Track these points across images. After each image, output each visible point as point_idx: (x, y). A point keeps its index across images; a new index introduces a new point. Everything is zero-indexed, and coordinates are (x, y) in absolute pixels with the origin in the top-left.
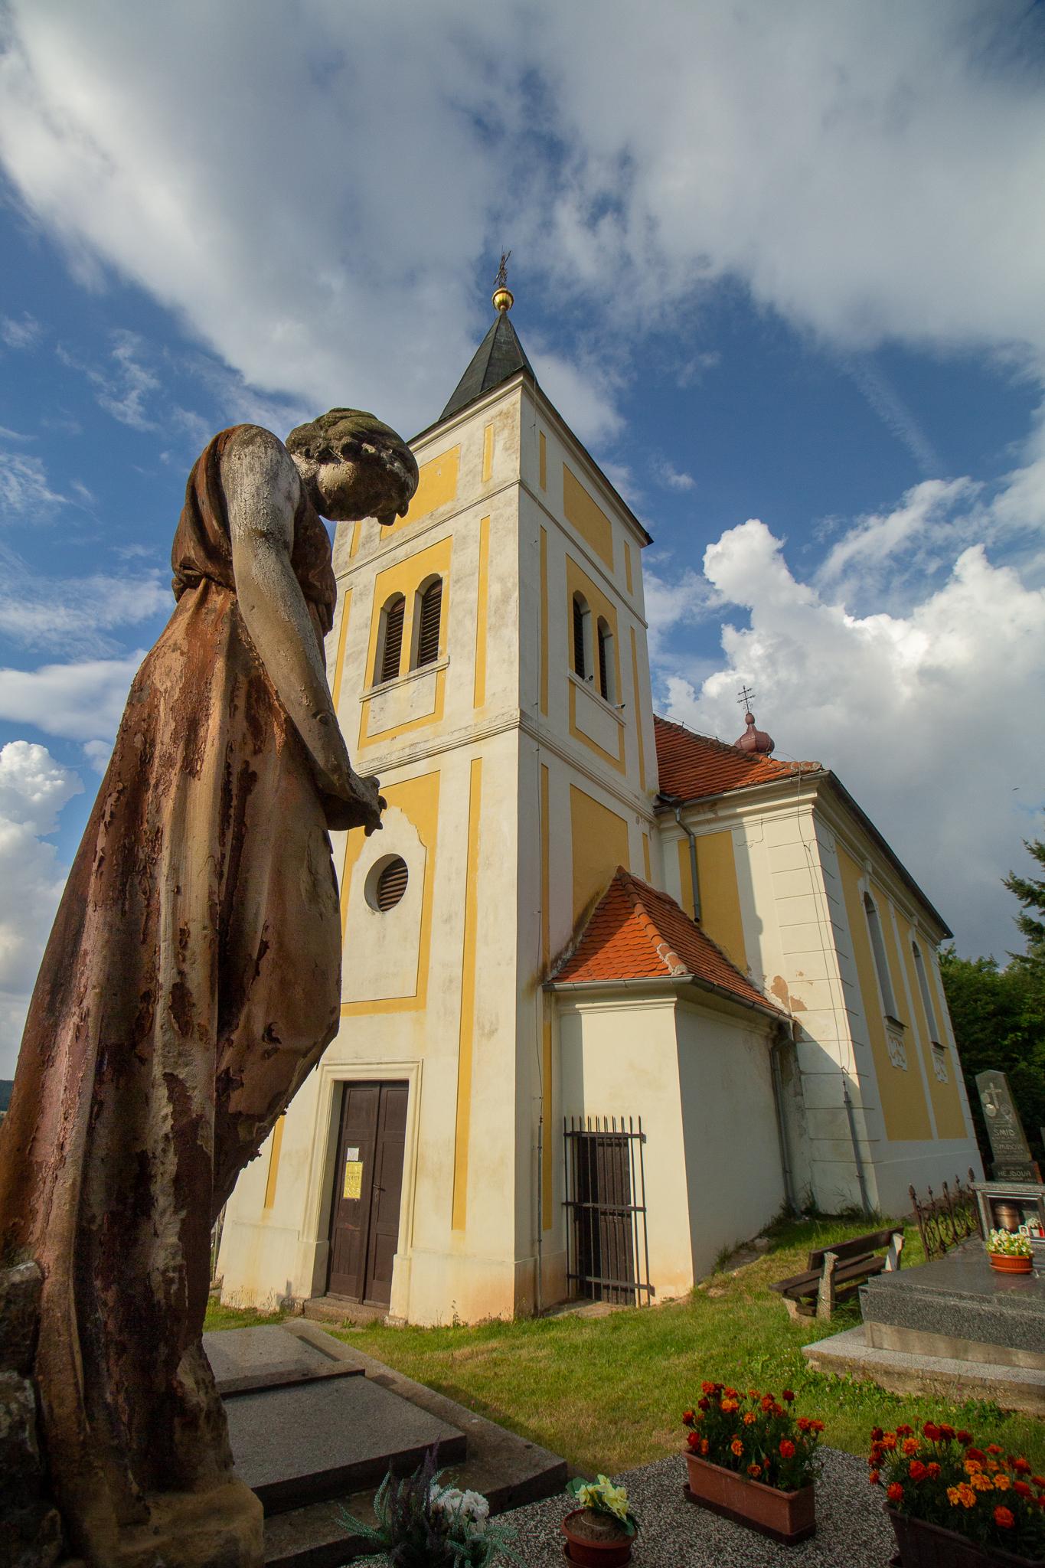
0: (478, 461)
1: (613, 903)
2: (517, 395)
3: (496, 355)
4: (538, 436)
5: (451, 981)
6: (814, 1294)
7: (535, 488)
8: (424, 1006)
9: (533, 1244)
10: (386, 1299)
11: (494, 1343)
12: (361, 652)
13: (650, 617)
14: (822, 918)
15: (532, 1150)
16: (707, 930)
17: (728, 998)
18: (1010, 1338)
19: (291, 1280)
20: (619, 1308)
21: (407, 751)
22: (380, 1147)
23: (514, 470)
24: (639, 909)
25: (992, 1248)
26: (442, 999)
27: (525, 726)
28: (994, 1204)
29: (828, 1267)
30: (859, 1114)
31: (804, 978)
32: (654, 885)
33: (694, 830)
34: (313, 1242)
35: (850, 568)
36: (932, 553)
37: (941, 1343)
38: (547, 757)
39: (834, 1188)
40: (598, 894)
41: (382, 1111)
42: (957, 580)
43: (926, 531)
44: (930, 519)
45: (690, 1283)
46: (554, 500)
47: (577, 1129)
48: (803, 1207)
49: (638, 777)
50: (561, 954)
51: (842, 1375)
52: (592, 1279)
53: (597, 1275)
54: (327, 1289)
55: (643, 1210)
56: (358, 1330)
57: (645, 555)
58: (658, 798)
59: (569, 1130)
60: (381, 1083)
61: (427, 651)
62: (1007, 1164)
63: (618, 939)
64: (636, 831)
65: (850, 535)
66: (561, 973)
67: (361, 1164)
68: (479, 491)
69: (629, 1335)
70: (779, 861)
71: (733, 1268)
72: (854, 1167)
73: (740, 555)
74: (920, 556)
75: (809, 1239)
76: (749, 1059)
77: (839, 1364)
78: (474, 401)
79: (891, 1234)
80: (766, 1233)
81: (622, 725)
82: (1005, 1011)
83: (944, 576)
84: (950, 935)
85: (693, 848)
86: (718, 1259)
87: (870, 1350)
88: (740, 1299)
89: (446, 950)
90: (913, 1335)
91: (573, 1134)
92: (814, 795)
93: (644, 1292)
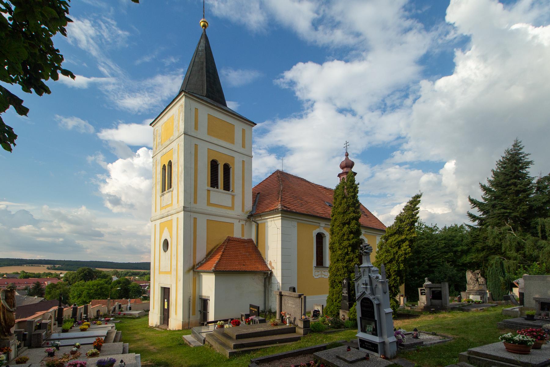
2: (184, 97)
16: (259, 249)
26: (174, 273)
34: (159, 316)
61: (170, 186)
66: (194, 270)
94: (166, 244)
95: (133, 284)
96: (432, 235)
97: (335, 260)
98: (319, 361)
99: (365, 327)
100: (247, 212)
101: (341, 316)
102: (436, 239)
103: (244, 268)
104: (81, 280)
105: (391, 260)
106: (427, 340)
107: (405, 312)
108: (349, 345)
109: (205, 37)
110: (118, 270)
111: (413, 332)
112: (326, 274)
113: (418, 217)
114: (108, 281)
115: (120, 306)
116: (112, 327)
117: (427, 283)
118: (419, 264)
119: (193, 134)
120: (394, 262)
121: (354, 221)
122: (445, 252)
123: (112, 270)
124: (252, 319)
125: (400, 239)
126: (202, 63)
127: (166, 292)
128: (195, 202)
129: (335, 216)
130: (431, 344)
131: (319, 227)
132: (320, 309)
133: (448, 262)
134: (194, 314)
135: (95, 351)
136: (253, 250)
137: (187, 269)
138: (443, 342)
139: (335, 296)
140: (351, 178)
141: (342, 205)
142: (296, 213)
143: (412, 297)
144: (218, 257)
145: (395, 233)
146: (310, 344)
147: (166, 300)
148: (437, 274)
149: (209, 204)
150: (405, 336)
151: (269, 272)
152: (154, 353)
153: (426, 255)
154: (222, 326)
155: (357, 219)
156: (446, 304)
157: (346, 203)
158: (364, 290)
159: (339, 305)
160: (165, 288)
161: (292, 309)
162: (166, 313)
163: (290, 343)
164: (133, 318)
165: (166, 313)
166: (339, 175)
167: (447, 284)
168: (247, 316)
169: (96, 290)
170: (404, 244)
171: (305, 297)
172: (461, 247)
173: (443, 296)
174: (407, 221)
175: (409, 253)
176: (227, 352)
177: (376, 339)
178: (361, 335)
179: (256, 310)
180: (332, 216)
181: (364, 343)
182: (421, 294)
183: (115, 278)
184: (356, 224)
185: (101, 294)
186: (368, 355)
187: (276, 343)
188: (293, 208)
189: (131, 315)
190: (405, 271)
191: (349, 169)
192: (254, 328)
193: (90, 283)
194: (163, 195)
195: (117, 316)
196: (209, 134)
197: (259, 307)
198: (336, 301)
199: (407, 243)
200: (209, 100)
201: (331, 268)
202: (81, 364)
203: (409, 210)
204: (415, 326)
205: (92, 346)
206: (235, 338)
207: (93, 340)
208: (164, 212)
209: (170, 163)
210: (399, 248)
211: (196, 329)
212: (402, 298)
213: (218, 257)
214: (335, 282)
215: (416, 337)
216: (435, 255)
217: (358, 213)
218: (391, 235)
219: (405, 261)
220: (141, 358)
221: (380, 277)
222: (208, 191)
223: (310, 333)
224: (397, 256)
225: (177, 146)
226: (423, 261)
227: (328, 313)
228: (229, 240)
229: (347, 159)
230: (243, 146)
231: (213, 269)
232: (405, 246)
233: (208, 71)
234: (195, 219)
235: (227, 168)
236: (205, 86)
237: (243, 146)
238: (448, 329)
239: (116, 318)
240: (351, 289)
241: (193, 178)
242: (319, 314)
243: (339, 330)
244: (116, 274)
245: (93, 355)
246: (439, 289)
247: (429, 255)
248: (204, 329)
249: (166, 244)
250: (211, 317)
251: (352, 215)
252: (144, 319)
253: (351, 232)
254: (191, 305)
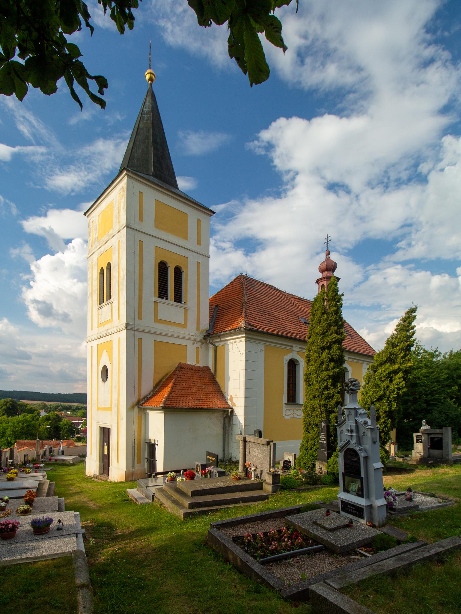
2: (126, 178)
3: (141, 126)
16: (218, 380)
21: (106, 332)
26: (115, 409)
34: (98, 463)
38: (139, 335)
40: (167, 374)
66: (139, 405)
92: (244, 335)
94: (105, 372)
95: (65, 420)
96: (432, 362)
97: (312, 396)
98: (292, 527)
99: (349, 485)
100: (202, 331)
101: (317, 469)
102: (438, 367)
103: (199, 404)
104: (3, 415)
105: (380, 396)
106: (423, 503)
107: (397, 465)
108: (329, 507)
109: (151, 94)
110: (47, 403)
111: (406, 492)
112: (299, 414)
113: (415, 340)
114: (35, 416)
115: (51, 449)
116: (44, 476)
117: (425, 427)
118: (415, 401)
119: (137, 227)
120: (384, 401)
121: (337, 345)
122: (447, 386)
123: (40, 402)
124: (209, 471)
125: (391, 369)
126: (148, 131)
127: (105, 434)
128: (140, 318)
129: (312, 338)
130: (428, 508)
131: (292, 351)
132: (291, 458)
133: (452, 398)
134: (139, 462)
135: (26, 507)
136: (210, 380)
137: (131, 404)
138: (442, 506)
139: (309, 443)
140: (333, 287)
141: (321, 324)
142: (264, 333)
143: (405, 445)
144: (167, 390)
145: (385, 362)
146: (279, 504)
147: (105, 444)
148: (436, 414)
149: (157, 320)
150: (397, 498)
151: (230, 410)
152: (93, 511)
153: (424, 390)
154: (173, 479)
155: (339, 342)
156: (448, 455)
157: (326, 320)
158: (349, 438)
159: (315, 455)
160: (104, 428)
161: (258, 459)
162: (106, 461)
163: (256, 503)
164: (67, 465)
165: (106, 461)
166: (318, 282)
167: (450, 429)
168: (204, 467)
169: (22, 428)
170: (397, 377)
171: (274, 445)
173: (444, 445)
174: (401, 345)
175: (403, 388)
176: (181, 513)
177: (362, 502)
178: (344, 496)
179: (214, 459)
180: (309, 338)
181: (347, 506)
182: (417, 442)
183: (43, 414)
184: (339, 349)
185: (28, 433)
186: (351, 522)
187: (239, 503)
188: (261, 327)
189: (64, 460)
190: (398, 411)
191: (331, 273)
192: (213, 483)
193: (16, 418)
194: (101, 308)
195: (50, 462)
196: (156, 226)
197: (218, 456)
198: (311, 449)
199: (401, 374)
200: (156, 180)
201: (306, 407)
202: (13, 524)
203: (401, 330)
204: (409, 484)
205: (22, 501)
206: (190, 494)
207: (24, 493)
208: (103, 330)
209: (109, 266)
210: (391, 381)
211: (142, 482)
212: (392, 446)
213: (167, 390)
214: (310, 425)
215: (410, 499)
216: (435, 389)
217: (341, 334)
218: (381, 364)
219: (398, 398)
220: (81, 517)
221: (369, 422)
222: (156, 302)
223: (280, 490)
224: (388, 393)
225: (117, 243)
226: (420, 398)
227: (302, 464)
228: (181, 368)
229: (328, 259)
230: (199, 243)
231: (162, 405)
232: (398, 378)
233: (155, 141)
234: (140, 339)
235: (178, 272)
236: (151, 161)
237: (199, 243)
238: (449, 489)
239: (48, 465)
240: (332, 435)
241: (137, 286)
242: (290, 465)
243: (315, 486)
244: (44, 408)
245: (25, 512)
246: (440, 436)
247: (427, 389)
248: (151, 482)
249: (105, 372)
250: (160, 467)
251: (334, 336)
252: (80, 466)
253: (332, 360)
254: (136, 451)
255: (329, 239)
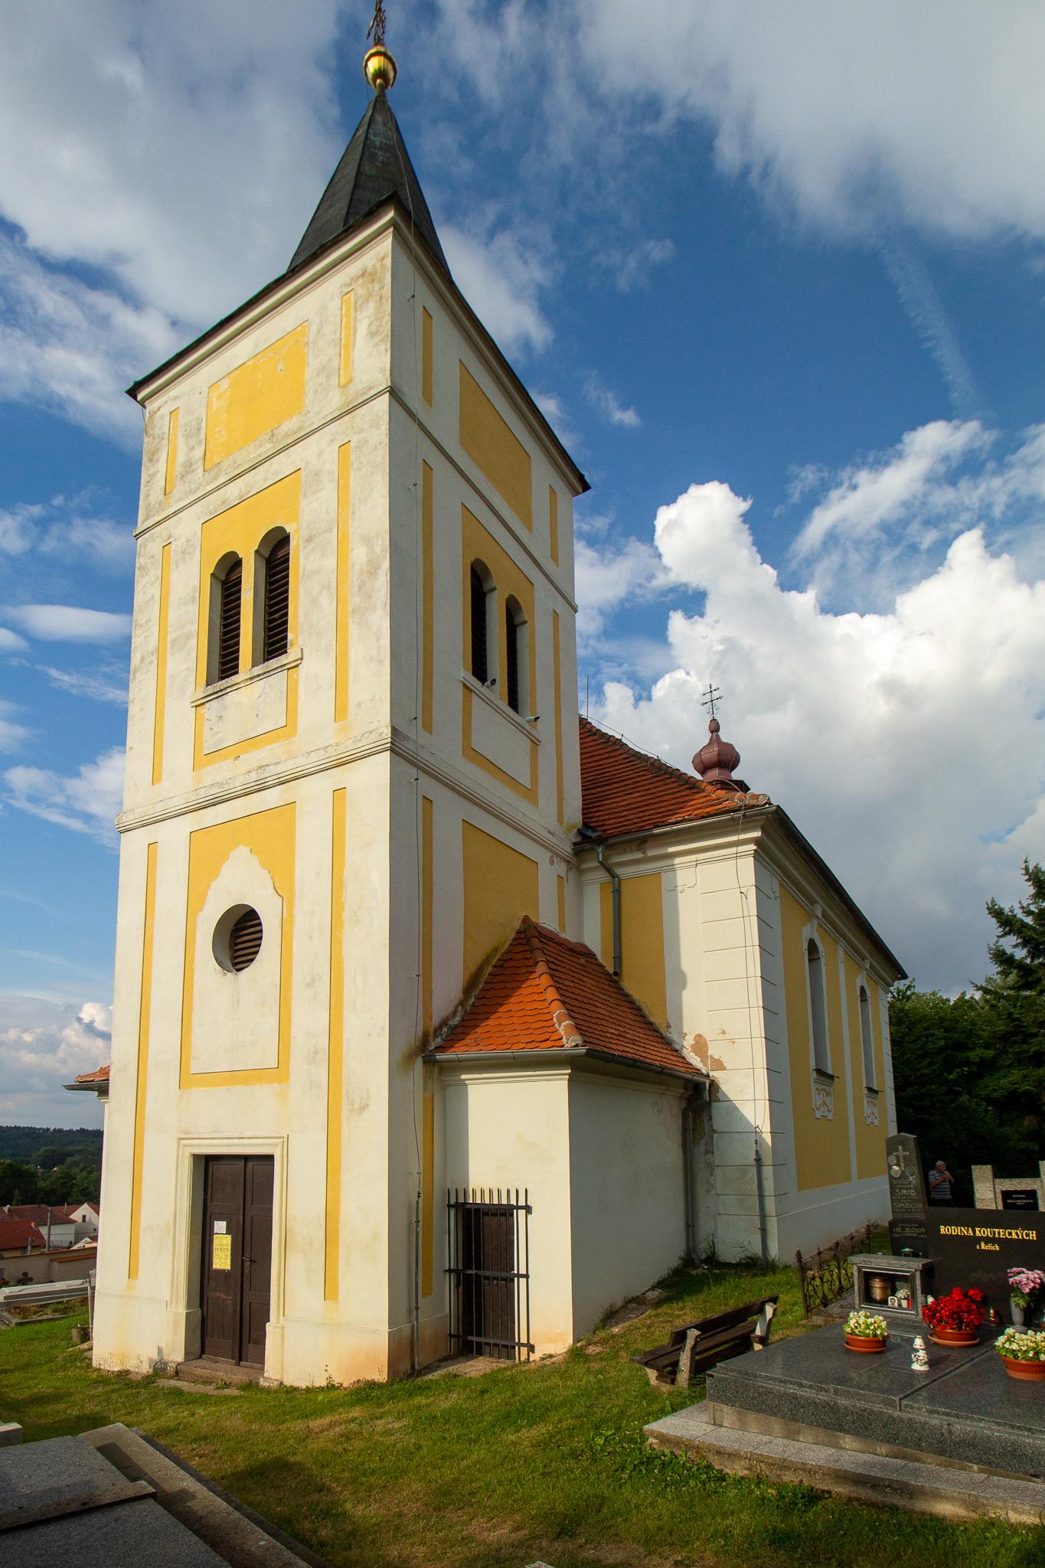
0: (332, 351)
1: (520, 956)
2: (386, 245)
4: (420, 311)
5: (316, 1053)
6: (675, 1364)
7: (415, 402)
8: (288, 1079)
9: (410, 1312)
10: (261, 1359)
11: (356, 1412)
12: (188, 637)
13: (579, 599)
14: (751, 973)
15: (410, 1224)
16: (627, 985)
17: (633, 1066)
18: (840, 1425)
19: (163, 1345)
20: (503, 1363)
21: (254, 776)
22: (248, 1220)
23: (383, 370)
24: (541, 968)
25: (849, 1330)
27: (399, 748)
28: (867, 1277)
29: (690, 1342)
30: (768, 1172)
31: (727, 1036)
32: (569, 935)
33: (619, 871)
34: (182, 1311)
35: (832, 539)
36: (929, 523)
37: (777, 1425)
39: (734, 1237)
40: (496, 949)
41: (249, 1186)
42: (950, 569)
43: (925, 495)
44: (932, 479)
45: (570, 1341)
46: (445, 422)
47: (461, 1200)
48: (704, 1256)
49: (556, 804)
50: (447, 1019)
51: (677, 1452)
52: (474, 1339)
53: (479, 1335)
54: (203, 1352)
55: (527, 1276)
56: (235, 1392)
57: (581, 517)
58: (580, 832)
59: (453, 1201)
60: (246, 1158)
61: (274, 641)
62: (904, 1221)
63: (513, 1004)
64: (549, 874)
65: (834, 494)
66: (437, 1051)
67: (229, 1237)
68: (334, 402)
69: (495, 1400)
70: (711, 915)
71: (617, 1324)
72: (757, 1220)
73: (699, 521)
74: (914, 527)
75: (700, 1291)
76: (655, 1124)
77: (677, 1442)
78: (336, 242)
79: (763, 1304)
80: (661, 1284)
81: (535, 743)
82: (960, 1046)
83: (937, 557)
84: (904, 977)
85: (617, 893)
86: (598, 1317)
87: (710, 1428)
88: (615, 1356)
89: (309, 1019)
90: (751, 1416)
91: (457, 1205)
93: (524, 1350)
127: (233, 1190)
151: (707, 1083)
172: (979, 1051)
191: (726, 772)
255: (716, 694)
